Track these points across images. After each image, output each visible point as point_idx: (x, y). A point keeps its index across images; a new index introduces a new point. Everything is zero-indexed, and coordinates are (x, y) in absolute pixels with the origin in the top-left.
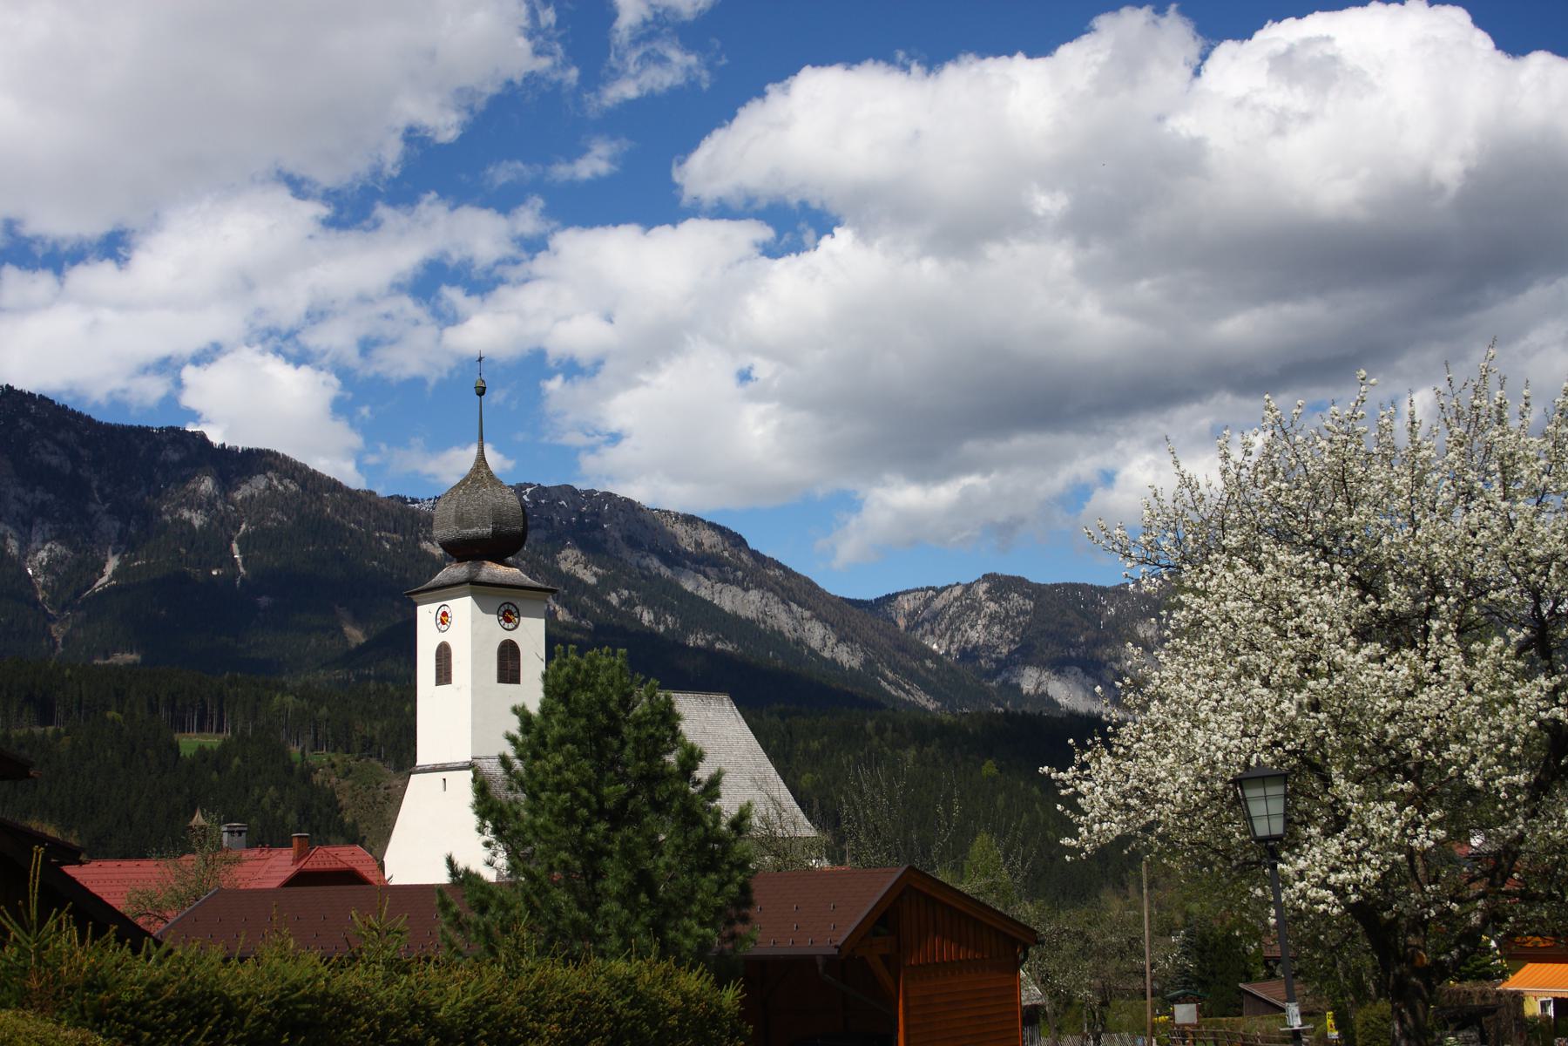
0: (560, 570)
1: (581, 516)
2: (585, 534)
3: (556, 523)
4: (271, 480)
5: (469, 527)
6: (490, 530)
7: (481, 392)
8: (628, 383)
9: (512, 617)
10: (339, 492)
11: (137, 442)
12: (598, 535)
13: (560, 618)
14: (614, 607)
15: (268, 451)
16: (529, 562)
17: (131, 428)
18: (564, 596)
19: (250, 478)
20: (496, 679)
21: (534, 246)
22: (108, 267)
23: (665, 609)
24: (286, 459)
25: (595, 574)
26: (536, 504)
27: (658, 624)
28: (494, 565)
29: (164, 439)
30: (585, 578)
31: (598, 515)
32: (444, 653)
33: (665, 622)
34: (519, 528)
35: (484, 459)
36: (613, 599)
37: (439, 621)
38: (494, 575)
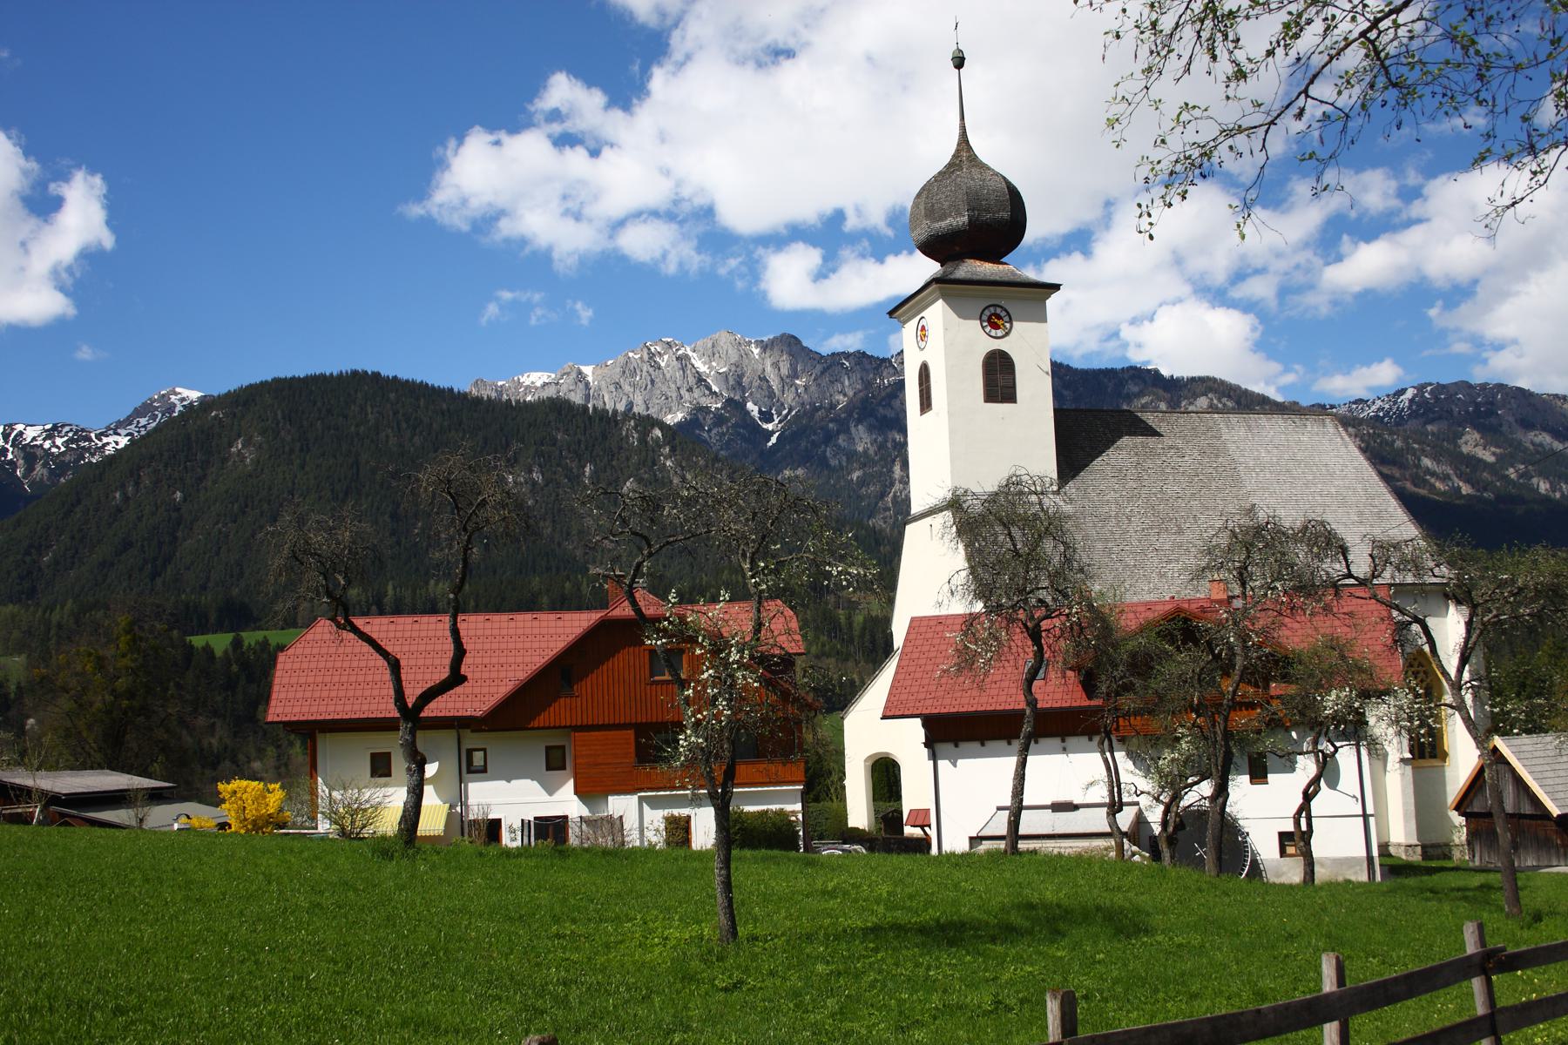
0: (1462, 453)
1: (1477, 405)
2: (1482, 420)
3: (1456, 414)
4: (1212, 399)
5: (942, 219)
6: (966, 219)
7: (959, 62)
8: (1503, 295)
9: (1000, 322)
10: (1267, 404)
11: (1106, 380)
12: (1493, 420)
13: (1464, 492)
14: (1513, 480)
15: (1208, 377)
16: (1433, 447)
17: (1100, 371)
18: (1466, 474)
19: (1195, 400)
21: (1410, 194)
22: (1077, 257)
23: (1560, 478)
24: (1222, 383)
25: (1494, 454)
26: (1437, 399)
27: (1554, 491)
29: (1126, 376)
30: (1484, 457)
31: (1492, 403)
32: (924, 373)
33: (1561, 490)
34: (1005, 215)
35: (970, 148)
36: (1511, 473)
38: (975, 273)
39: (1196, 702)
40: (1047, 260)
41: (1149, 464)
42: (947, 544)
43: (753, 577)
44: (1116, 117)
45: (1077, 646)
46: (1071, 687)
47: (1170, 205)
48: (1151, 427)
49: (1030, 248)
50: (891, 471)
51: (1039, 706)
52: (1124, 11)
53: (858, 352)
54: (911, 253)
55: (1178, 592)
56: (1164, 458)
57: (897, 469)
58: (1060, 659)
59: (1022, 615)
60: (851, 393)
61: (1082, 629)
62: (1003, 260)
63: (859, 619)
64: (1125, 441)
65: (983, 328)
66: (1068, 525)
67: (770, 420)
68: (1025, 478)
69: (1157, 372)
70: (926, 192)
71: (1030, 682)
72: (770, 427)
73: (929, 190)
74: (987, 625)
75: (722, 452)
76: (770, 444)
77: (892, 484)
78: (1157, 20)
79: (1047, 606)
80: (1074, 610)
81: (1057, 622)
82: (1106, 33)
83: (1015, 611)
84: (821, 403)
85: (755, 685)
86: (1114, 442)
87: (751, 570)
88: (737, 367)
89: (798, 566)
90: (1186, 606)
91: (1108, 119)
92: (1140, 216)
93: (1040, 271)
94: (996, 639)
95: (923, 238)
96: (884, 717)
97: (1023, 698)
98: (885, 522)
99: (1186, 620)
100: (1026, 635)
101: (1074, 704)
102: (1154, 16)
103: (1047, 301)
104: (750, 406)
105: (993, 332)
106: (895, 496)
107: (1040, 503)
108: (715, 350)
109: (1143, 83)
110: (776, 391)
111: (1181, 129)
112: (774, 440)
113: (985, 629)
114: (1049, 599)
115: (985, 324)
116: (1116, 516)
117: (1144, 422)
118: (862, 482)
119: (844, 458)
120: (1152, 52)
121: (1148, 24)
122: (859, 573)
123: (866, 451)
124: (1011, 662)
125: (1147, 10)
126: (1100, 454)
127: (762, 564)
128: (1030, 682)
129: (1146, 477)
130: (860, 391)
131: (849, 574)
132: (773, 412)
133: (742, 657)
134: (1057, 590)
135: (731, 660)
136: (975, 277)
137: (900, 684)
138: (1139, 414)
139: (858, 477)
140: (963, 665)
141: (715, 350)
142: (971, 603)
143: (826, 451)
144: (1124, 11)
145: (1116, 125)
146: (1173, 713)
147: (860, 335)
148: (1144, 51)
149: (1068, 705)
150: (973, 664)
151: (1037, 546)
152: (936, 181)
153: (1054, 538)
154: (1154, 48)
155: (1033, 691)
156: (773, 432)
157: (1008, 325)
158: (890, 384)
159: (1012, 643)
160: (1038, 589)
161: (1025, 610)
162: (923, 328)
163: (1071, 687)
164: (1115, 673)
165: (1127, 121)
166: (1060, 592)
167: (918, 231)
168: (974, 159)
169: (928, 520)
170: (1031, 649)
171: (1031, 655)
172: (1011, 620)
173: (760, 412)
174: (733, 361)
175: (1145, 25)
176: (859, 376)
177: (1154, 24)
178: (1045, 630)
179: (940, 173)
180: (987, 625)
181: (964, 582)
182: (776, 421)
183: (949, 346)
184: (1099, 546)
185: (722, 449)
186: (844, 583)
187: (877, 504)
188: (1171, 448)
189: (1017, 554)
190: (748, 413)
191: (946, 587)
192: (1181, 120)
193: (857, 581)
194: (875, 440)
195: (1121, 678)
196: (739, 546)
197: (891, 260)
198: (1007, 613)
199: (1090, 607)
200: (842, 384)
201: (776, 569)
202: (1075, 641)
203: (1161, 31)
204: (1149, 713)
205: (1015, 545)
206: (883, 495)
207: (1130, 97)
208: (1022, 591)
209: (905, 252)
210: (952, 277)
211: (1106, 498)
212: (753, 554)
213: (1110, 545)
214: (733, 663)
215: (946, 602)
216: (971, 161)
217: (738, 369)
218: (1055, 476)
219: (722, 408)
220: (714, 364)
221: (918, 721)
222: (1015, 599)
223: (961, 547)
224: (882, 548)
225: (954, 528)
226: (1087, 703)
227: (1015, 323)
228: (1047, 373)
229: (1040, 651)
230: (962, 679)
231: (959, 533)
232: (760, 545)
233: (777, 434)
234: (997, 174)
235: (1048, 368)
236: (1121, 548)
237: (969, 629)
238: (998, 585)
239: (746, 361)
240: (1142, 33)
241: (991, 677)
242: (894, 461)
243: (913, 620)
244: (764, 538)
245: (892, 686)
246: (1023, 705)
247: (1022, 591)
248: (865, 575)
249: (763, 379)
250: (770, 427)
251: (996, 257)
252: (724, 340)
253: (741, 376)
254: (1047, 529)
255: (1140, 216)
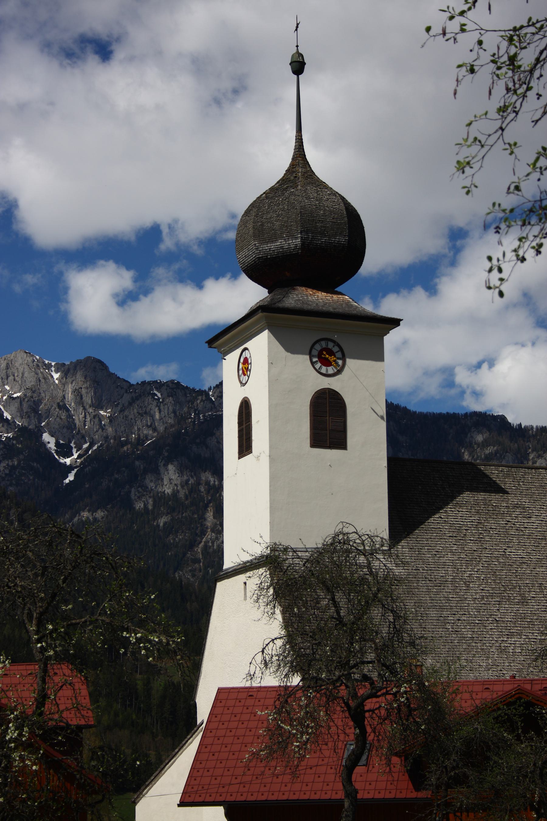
9: (332, 359)
17: (441, 415)
20: (309, 445)
22: (419, 293)
28: (310, 291)
34: (343, 239)
37: (241, 372)
39: (537, 799)
40: (384, 296)
41: (491, 524)
42: (262, 608)
43: (39, 641)
44: (467, 160)
45: (405, 730)
46: (396, 776)
47: (523, 260)
48: (495, 482)
49: (367, 280)
50: (203, 518)
51: (359, 796)
52: (480, 43)
53: (172, 381)
54: (235, 277)
55: (520, 670)
56: (508, 518)
57: (210, 515)
58: (385, 744)
59: (343, 692)
60: (161, 428)
61: (410, 711)
62: (338, 289)
63: (158, 684)
64: (466, 496)
65: (313, 363)
66: (399, 591)
67: (69, 454)
68: (353, 537)
69: (503, 419)
70: (255, 210)
71: (350, 769)
72: (68, 461)
73: (259, 208)
74: (304, 701)
75: (11, 488)
76: (67, 481)
77: (203, 533)
78: (515, 55)
79: (372, 683)
80: (403, 689)
81: (382, 701)
82: (459, 66)
83: (335, 688)
84: (127, 437)
85: (34, 768)
86: (453, 498)
87: (37, 632)
88: (34, 392)
89: (91, 630)
90: (528, 687)
91: (458, 162)
92: (490, 270)
93: (376, 301)
94: (314, 719)
95: (249, 260)
96: (182, 804)
97: (341, 787)
98: (193, 576)
99: (529, 705)
100: (347, 714)
101: (399, 796)
102: (513, 50)
103: (386, 338)
104: (46, 437)
105: (324, 370)
106: (206, 546)
107: (369, 566)
108: (10, 371)
109: (498, 124)
110: (77, 422)
111: (537, 175)
112: (71, 477)
113: (300, 706)
114: (374, 676)
115: (315, 360)
116: (453, 581)
117: (487, 476)
118: (169, 529)
119: (151, 501)
120: (508, 90)
121: (505, 58)
122: (160, 641)
123: (175, 494)
124: (330, 744)
125: (504, 44)
126: (437, 510)
127: (50, 627)
128: (350, 769)
129: (487, 538)
130: (172, 426)
131: (150, 641)
132: (72, 445)
133: (20, 735)
134: (384, 665)
135: (8, 738)
136: (305, 307)
137: (202, 766)
138: (482, 468)
139: (165, 523)
140: (275, 747)
141: (10, 371)
142: (287, 676)
143: (130, 492)
144: (480, 43)
145: (467, 169)
146: (511, 811)
147: (174, 367)
148: (500, 89)
149: (392, 796)
150: (286, 747)
151: (365, 613)
152: (267, 197)
153: (383, 606)
154: (511, 85)
155: (353, 779)
156: (70, 468)
157: (340, 362)
158: (205, 419)
159: (331, 724)
160: (363, 663)
161: (347, 687)
162: (246, 361)
163: (396, 776)
164: (447, 763)
165: (479, 164)
166: (387, 667)
167: (245, 252)
168: (309, 174)
169: (241, 578)
170: (353, 732)
171: (352, 737)
172: (331, 698)
173: (57, 444)
174: (29, 385)
175: (502, 60)
176: (171, 409)
177: (512, 59)
178: (368, 711)
179: (272, 189)
180: (304, 701)
181: (280, 651)
182: (75, 456)
183: (273, 382)
184: (433, 613)
185: (11, 485)
186: (143, 652)
187: (185, 554)
188: (516, 506)
189: (341, 622)
190: (44, 445)
191: (259, 658)
192: (538, 165)
193: (158, 650)
194: (187, 482)
195: (453, 768)
196: (25, 605)
197: (210, 284)
198: (327, 689)
199: (421, 686)
200: (152, 416)
201: (66, 633)
202: (403, 724)
203: (520, 67)
204: (484, 810)
205: (338, 613)
206: (192, 545)
207: (483, 138)
208: (344, 665)
209: (229, 275)
210: (280, 305)
211: (442, 560)
212: (41, 614)
213: (445, 613)
214: (11, 740)
215: (258, 674)
216: (307, 178)
217: (35, 395)
218: (386, 535)
219: (14, 438)
220: (7, 387)
221: (220, 810)
222: (337, 673)
223: (278, 611)
224: (188, 604)
225: (271, 591)
226: (414, 795)
227: (348, 360)
228: (382, 418)
229: (363, 732)
230: (273, 763)
231: (276, 595)
232: (49, 604)
233: (76, 470)
234: (335, 194)
235: (382, 410)
236: (457, 616)
237: (283, 707)
238: (318, 657)
239: (44, 386)
240: (499, 68)
241: (306, 760)
242: (206, 506)
243: (220, 691)
244: (54, 596)
245: (193, 768)
246: (340, 795)
247: (344, 665)
248: (168, 644)
249: (62, 407)
250: (68, 461)
251: (330, 288)
252: (20, 361)
253: (37, 403)
254: (375, 595)
255: (490, 270)
